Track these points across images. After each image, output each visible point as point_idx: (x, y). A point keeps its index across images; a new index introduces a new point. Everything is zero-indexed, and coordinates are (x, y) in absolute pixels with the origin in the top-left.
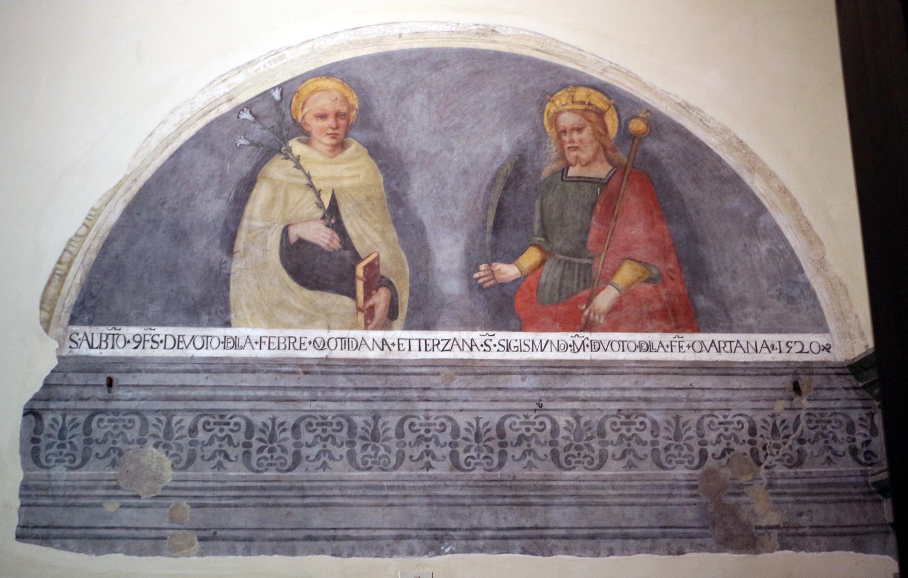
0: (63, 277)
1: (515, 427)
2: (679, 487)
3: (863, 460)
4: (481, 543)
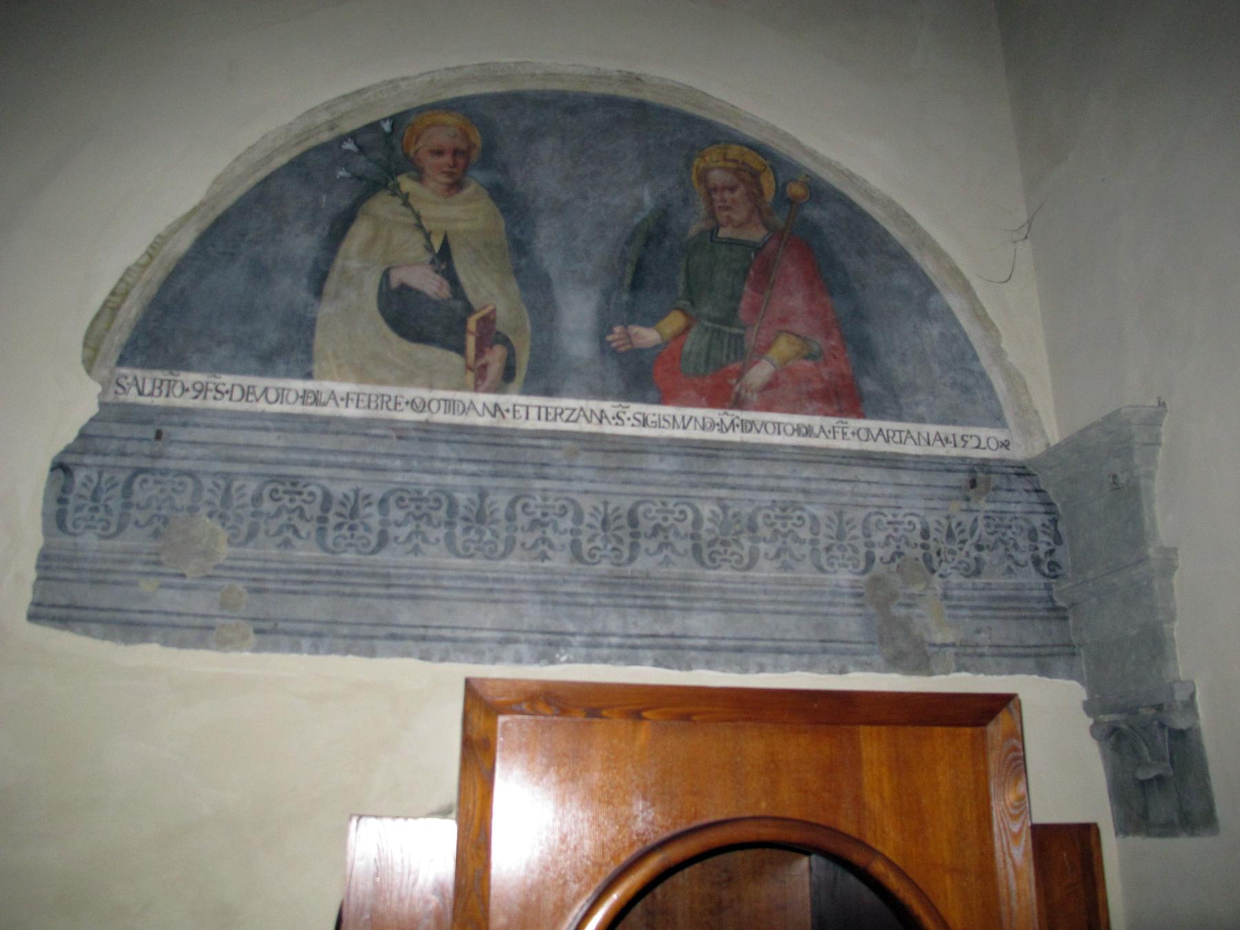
0: (115, 310)
1: (650, 515)
2: (842, 595)
3: (1047, 571)
4: (605, 652)
